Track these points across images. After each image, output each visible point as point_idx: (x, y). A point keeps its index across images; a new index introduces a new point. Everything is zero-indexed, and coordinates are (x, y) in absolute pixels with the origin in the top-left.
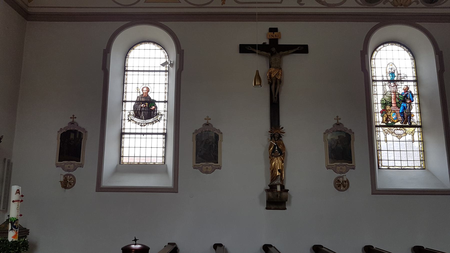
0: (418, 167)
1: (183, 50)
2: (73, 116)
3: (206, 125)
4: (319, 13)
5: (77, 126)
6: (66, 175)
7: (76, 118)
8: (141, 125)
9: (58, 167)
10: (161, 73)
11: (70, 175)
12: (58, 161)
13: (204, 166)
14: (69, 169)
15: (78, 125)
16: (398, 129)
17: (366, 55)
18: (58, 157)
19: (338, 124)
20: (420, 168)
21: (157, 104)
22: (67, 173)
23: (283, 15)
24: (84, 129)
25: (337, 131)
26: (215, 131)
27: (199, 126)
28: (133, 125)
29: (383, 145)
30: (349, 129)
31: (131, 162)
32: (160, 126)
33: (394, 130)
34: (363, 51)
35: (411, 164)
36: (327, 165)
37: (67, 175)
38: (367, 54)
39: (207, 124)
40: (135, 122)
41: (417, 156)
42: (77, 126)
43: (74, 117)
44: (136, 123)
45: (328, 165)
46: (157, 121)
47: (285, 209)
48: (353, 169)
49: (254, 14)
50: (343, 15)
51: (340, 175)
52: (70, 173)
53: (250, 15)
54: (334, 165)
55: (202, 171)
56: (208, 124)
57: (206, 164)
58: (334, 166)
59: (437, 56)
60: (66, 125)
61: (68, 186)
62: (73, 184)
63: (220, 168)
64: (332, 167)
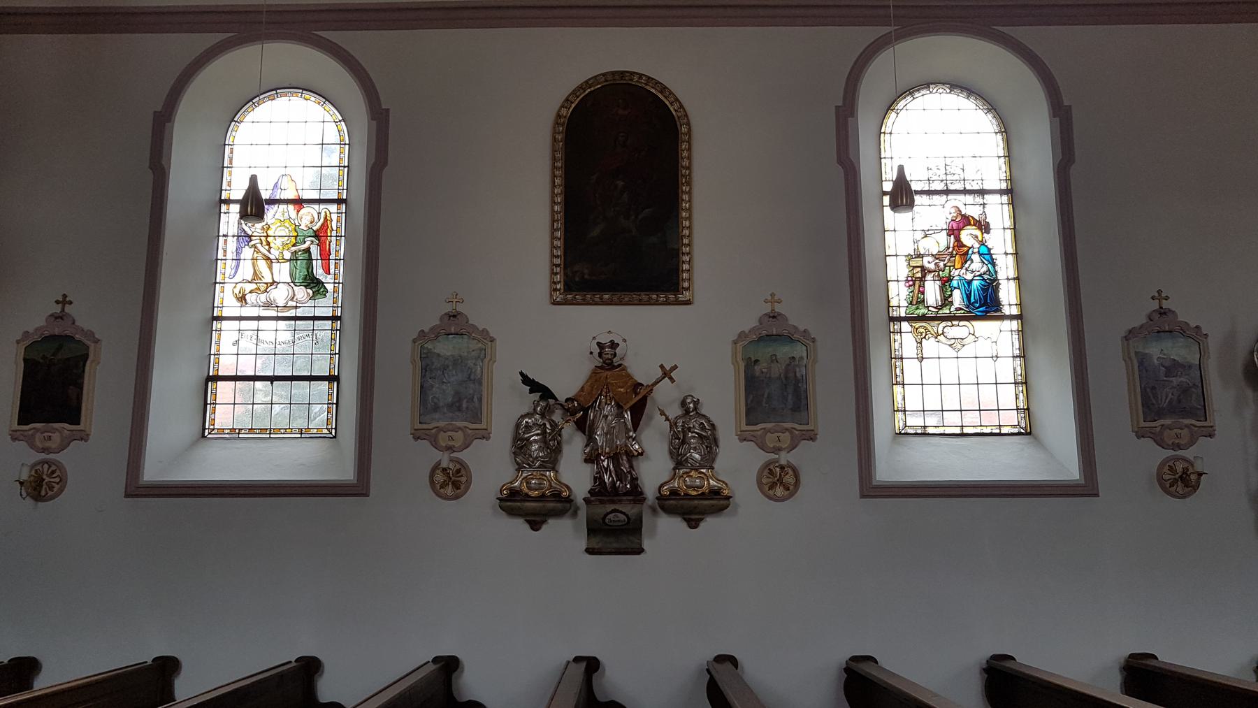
1: (387, 110)
2: (65, 296)
3: (450, 316)
4: (327, 7)
6: (39, 463)
11: (49, 463)
14: (451, 443)
15: (76, 324)
16: (953, 326)
18: (16, 413)
19: (773, 316)
20: (1016, 431)
24: (91, 334)
25: (769, 334)
26: (473, 335)
29: (911, 371)
33: (944, 327)
34: (160, 112)
35: (990, 420)
36: (739, 429)
37: (43, 462)
38: (853, 117)
39: (773, 316)
41: (1009, 397)
42: (467, 323)
45: (743, 429)
46: (930, 308)
47: (640, 551)
48: (811, 439)
50: (327, 10)
52: (52, 456)
54: (432, 429)
56: (455, 314)
57: (774, 426)
58: (759, 433)
59: (374, 122)
61: (43, 493)
63: (486, 437)
64: (1153, 432)
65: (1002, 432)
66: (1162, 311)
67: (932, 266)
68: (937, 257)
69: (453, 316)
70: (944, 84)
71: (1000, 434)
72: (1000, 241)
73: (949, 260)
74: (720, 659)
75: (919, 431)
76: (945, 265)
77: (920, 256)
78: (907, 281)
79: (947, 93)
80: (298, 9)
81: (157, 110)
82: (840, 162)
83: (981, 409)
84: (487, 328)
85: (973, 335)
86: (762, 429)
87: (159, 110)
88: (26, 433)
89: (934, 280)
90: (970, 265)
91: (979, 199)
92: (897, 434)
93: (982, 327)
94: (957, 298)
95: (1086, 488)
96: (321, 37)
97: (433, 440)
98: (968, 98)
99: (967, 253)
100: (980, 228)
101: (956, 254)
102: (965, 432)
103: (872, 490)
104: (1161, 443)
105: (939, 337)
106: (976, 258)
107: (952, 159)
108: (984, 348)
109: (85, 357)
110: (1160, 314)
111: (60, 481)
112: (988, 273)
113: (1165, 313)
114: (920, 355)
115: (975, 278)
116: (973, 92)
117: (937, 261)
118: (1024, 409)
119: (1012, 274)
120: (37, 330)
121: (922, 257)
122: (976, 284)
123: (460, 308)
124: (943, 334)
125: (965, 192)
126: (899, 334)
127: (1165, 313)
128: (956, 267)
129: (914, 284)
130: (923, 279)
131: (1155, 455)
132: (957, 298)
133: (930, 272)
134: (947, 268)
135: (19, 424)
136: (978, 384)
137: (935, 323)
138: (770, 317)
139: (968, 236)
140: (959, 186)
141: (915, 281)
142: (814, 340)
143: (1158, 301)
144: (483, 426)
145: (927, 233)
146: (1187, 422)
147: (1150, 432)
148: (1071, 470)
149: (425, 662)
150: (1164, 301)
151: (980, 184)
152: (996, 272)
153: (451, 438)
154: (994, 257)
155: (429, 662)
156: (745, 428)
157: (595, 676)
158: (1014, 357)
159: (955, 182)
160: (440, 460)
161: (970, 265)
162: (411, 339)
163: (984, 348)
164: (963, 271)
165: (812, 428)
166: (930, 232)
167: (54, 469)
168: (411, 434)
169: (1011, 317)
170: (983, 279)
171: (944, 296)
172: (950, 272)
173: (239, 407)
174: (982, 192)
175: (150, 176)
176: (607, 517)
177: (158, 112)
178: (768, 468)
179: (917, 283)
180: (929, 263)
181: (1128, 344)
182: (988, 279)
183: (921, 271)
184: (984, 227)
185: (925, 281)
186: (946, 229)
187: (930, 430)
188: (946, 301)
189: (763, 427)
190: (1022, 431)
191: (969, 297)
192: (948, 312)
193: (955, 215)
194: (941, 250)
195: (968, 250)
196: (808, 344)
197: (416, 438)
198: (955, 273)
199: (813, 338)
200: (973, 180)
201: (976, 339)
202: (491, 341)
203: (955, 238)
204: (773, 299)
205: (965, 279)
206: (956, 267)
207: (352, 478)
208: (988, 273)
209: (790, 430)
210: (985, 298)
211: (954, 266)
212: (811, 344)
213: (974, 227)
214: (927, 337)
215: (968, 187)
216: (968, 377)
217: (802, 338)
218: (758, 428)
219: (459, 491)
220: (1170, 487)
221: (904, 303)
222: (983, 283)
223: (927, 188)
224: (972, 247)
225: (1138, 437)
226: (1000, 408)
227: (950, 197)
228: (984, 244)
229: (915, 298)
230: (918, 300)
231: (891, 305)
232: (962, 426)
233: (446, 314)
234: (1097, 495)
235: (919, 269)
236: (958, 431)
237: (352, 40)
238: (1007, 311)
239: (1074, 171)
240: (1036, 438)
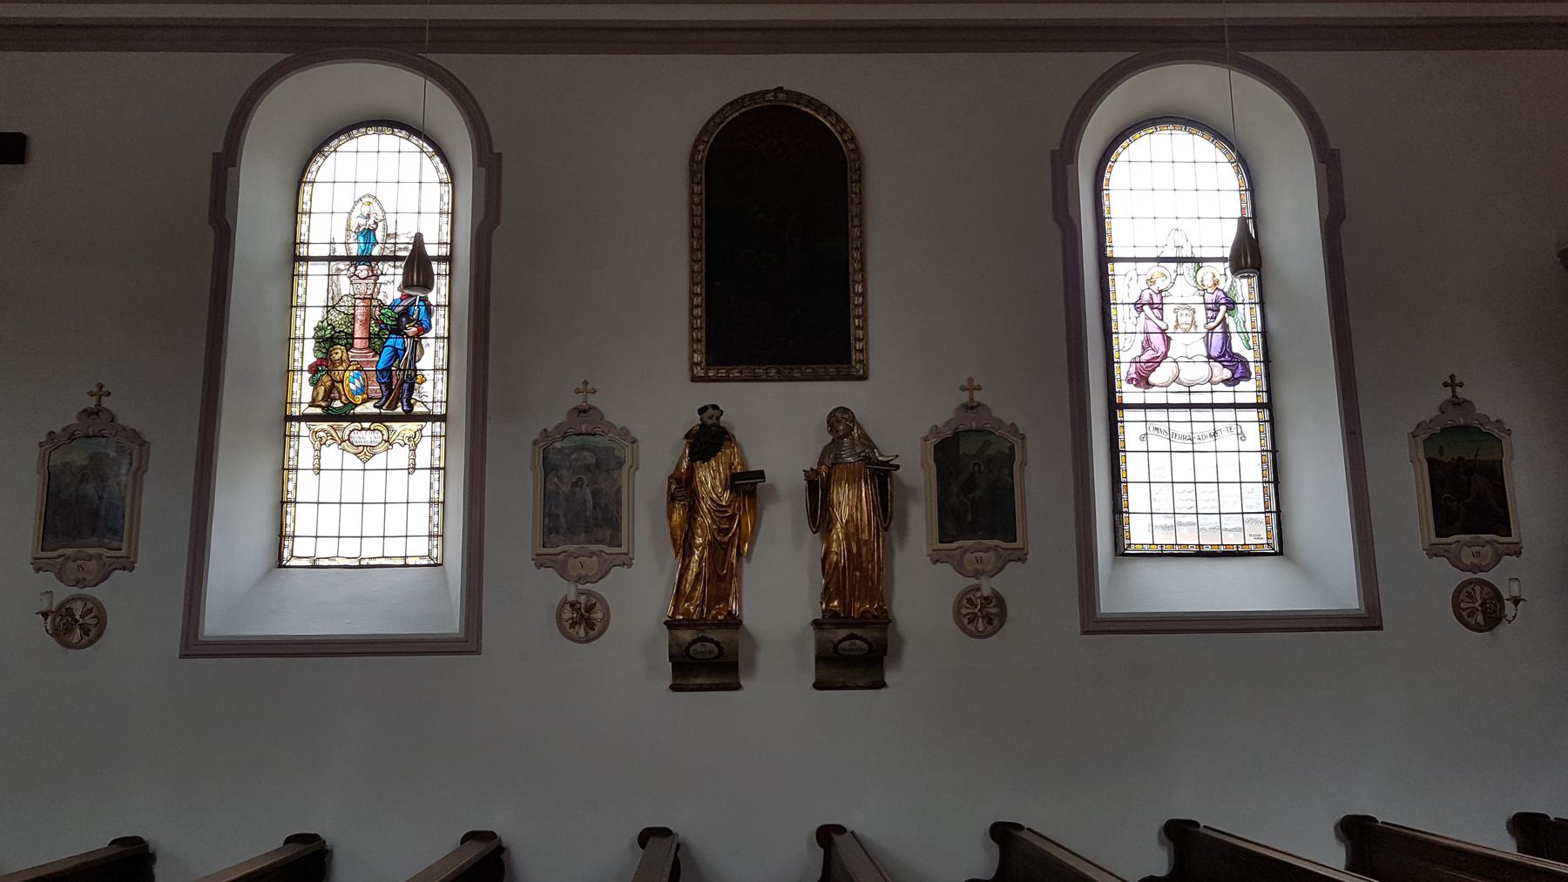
1: (500, 154)
3: (580, 412)
16: (363, 429)
20: (425, 562)
24: (625, 432)
27: (555, 417)
30: (1493, 418)
35: (395, 549)
38: (1072, 163)
63: (627, 563)
66: (1456, 400)
69: (583, 411)
82: (1056, 220)
84: (1015, 422)
95: (1368, 620)
103: (1095, 624)
105: (343, 444)
109: (1011, 458)
113: (1459, 404)
123: (593, 400)
127: (1459, 404)
135: (1438, 536)
138: (967, 408)
142: (1023, 438)
144: (623, 549)
146: (91, 551)
147: (1445, 551)
148: (1345, 595)
150: (1458, 387)
158: (432, 469)
160: (566, 596)
162: (532, 440)
163: (399, 456)
168: (533, 560)
175: (210, 234)
178: (966, 598)
181: (1416, 441)
196: (1016, 442)
197: (539, 566)
204: (971, 387)
212: (1020, 441)
217: (617, 437)
220: (969, 623)
226: (1241, 515)
232: (406, 557)
233: (574, 408)
234: (1380, 628)
236: (401, 562)
237: (452, 62)
240: (1286, 556)
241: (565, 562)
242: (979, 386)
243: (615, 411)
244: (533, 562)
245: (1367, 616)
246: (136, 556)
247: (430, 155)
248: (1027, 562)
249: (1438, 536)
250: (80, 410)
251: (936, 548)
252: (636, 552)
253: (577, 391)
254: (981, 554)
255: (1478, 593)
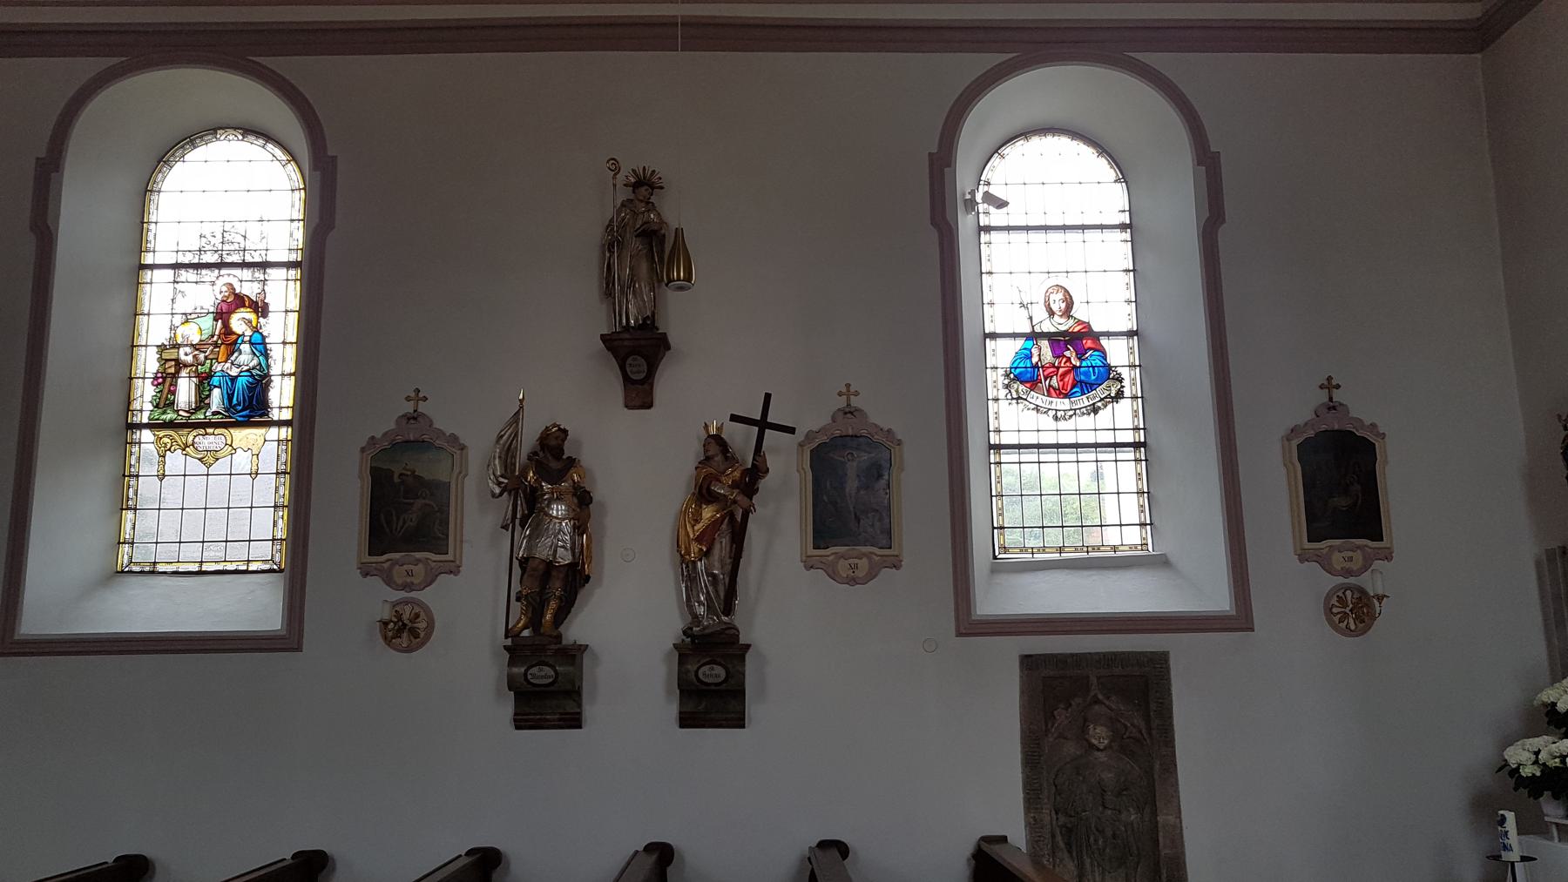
0: (259, 563)
1: (334, 158)
3: (409, 419)
5: (430, 426)
7: (425, 399)
8: (1056, 418)
9: (367, 574)
10: (1108, 234)
12: (369, 555)
13: (397, 567)
14: (409, 580)
16: (207, 434)
17: (946, 169)
19: (849, 411)
20: (267, 567)
21: (1104, 342)
22: (402, 594)
23: (764, 26)
24: (454, 439)
25: (843, 434)
26: (437, 442)
27: (383, 424)
28: (1029, 419)
30: (1368, 422)
31: (1032, 548)
32: (1122, 418)
33: (195, 436)
35: (237, 553)
36: (804, 555)
37: (406, 602)
38: (58, 171)
39: (413, 417)
40: (1034, 406)
43: (421, 395)
44: (1037, 409)
45: (809, 554)
46: (181, 413)
48: (895, 566)
49: (668, 24)
51: (1338, 582)
53: (929, 28)
55: (833, 575)
58: (831, 558)
60: (825, 420)
62: (426, 634)
63: (455, 571)
65: (250, 569)
67: (189, 359)
68: (197, 347)
70: (235, 129)
71: (246, 572)
72: (282, 328)
73: (212, 351)
74: (824, 845)
75: (147, 569)
76: (206, 358)
77: (177, 346)
78: (156, 378)
79: (238, 140)
80: (1301, 25)
81: (40, 156)
82: (934, 223)
83: (252, 539)
85: (231, 446)
86: (833, 554)
87: (43, 156)
88: (823, 560)
89: (190, 377)
90: (237, 358)
91: (259, 275)
92: (118, 572)
93: (242, 436)
94: (216, 399)
96: (264, 67)
97: (385, 576)
98: (195, 148)
99: (235, 342)
100: (256, 311)
101: (222, 344)
102: (203, 569)
104: (389, 582)
105: (187, 449)
106: (245, 348)
107: (233, 224)
108: (242, 461)
110: (1329, 409)
111: (1331, 608)
112: (258, 367)
113: (1334, 408)
114: (161, 472)
115: (242, 374)
116: (272, 139)
117: (196, 352)
118: (281, 539)
119: (290, 366)
120: (385, 434)
121: (178, 348)
122: (242, 382)
124: (193, 445)
125: (244, 265)
126: (137, 446)
127: (1334, 408)
128: (220, 360)
129: (164, 382)
130: (175, 376)
131: (378, 599)
132: (216, 399)
133: (186, 366)
134: (209, 361)
135: (816, 547)
136: (1118, 493)
137: (185, 431)
139: (238, 323)
140: (236, 258)
141: (166, 377)
143: (1327, 390)
144: (450, 557)
145: (189, 317)
146: (418, 555)
149: (456, 855)
150: (1335, 390)
151: (263, 253)
152: (268, 366)
153: (409, 574)
154: (268, 346)
155: (460, 856)
156: (811, 551)
157: (670, 870)
159: (232, 253)
161: (237, 358)
164: (228, 365)
165: (896, 553)
166: (193, 316)
167: (1336, 599)
169: (280, 423)
170: (252, 376)
171: (200, 397)
172: (211, 366)
173: (233, 532)
174: (264, 265)
175: (934, 235)
176: (529, 672)
177: (42, 159)
179: (169, 380)
180: (185, 355)
182: (257, 375)
183: (176, 365)
184: (261, 309)
185: (179, 377)
186: (213, 313)
187: (160, 568)
188: (202, 402)
189: (1329, 544)
190: (275, 567)
191: (230, 399)
192: (203, 417)
193: (227, 294)
194: (204, 337)
195: (238, 339)
197: (366, 574)
198: (218, 367)
199: (899, 440)
200: (255, 251)
201: (234, 451)
202: (899, 445)
203: (223, 323)
205: (229, 375)
206: (220, 360)
207: (978, 613)
208: (258, 367)
209: (868, 555)
210: (251, 398)
211: (217, 359)
213: (249, 310)
214: (172, 449)
215: (249, 259)
216: (1070, 486)
218: (829, 553)
219: (418, 640)
221: (148, 407)
222: (251, 380)
223: (196, 261)
224: (243, 335)
225: (1301, 561)
227: (223, 272)
228: (258, 331)
229: (163, 399)
230: (165, 401)
231: (131, 408)
233: (403, 416)
235: (173, 363)
236: (194, 567)
237: (292, 66)
238: (275, 415)
239: (1224, 235)
241: (391, 569)
242: (414, 391)
243: (443, 416)
244: (359, 571)
245: (287, 636)
246: (461, 562)
247: (283, 163)
248: (902, 569)
249: (816, 547)
250: (401, 414)
251: (365, 561)
252: (464, 559)
253: (408, 399)
254: (856, 561)
255: (1349, 598)
